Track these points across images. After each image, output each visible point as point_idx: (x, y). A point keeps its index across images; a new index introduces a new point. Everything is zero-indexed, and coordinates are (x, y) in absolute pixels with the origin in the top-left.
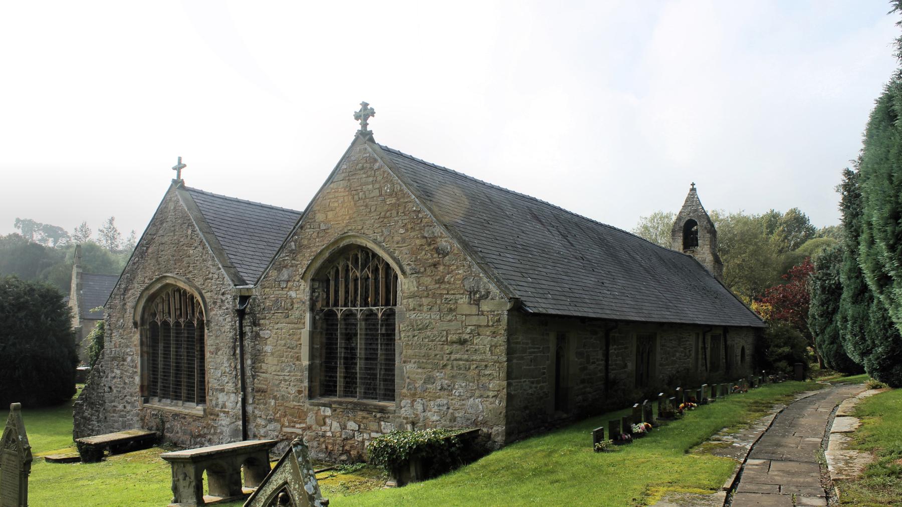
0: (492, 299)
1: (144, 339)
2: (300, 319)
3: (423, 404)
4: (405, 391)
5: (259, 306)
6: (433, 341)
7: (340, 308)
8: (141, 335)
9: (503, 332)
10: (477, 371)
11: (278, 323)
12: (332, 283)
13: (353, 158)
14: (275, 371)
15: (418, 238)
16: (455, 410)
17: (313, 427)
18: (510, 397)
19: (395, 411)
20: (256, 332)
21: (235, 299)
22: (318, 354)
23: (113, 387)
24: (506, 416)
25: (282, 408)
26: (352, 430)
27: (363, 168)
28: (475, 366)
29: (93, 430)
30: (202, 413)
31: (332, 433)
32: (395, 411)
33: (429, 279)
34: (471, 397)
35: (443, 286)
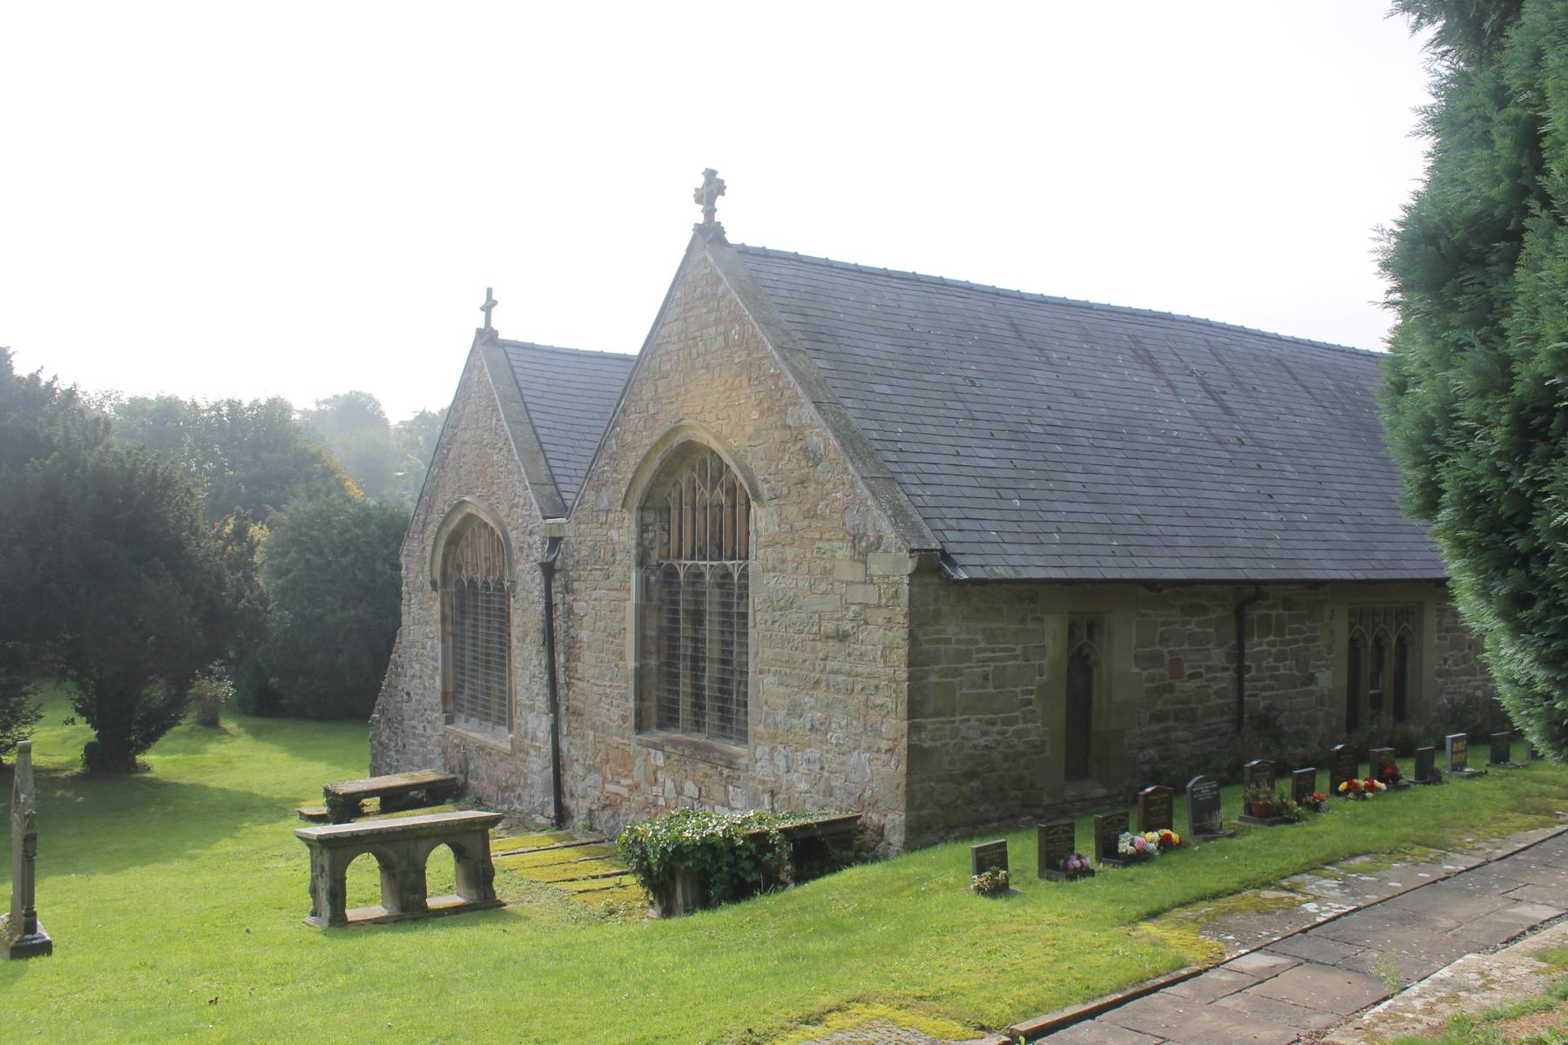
0: (886, 551)
1: (448, 611)
2: (625, 580)
3: (787, 757)
4: (761, 728)
5: (572, 556)
6: (801, 632)
7: (683, 562)
8: (443, 604)
9: (901, 619)
10: (862, 698)
11: (595, 589)
12: (674, 513)
13: (690, 278)
14: (593, 677)
15: (776, 427)
16: (831, 772)
17: (642, 786)
18: (917, 756)
19: (747, 766)
20: (569, 604)
21: (543, 543)
22: (653, 648)
23: (412, 693)
24: (906, 792)
25: (602, 746)
26: (691, 797)
27: (703, 296)
28: (860, 687)
29: (390, 766)
30: (508, 747)
31: (666, 800)
32: (747, 766)
33: (794, 509)
34: (855, 749)
35: (814, 524)
